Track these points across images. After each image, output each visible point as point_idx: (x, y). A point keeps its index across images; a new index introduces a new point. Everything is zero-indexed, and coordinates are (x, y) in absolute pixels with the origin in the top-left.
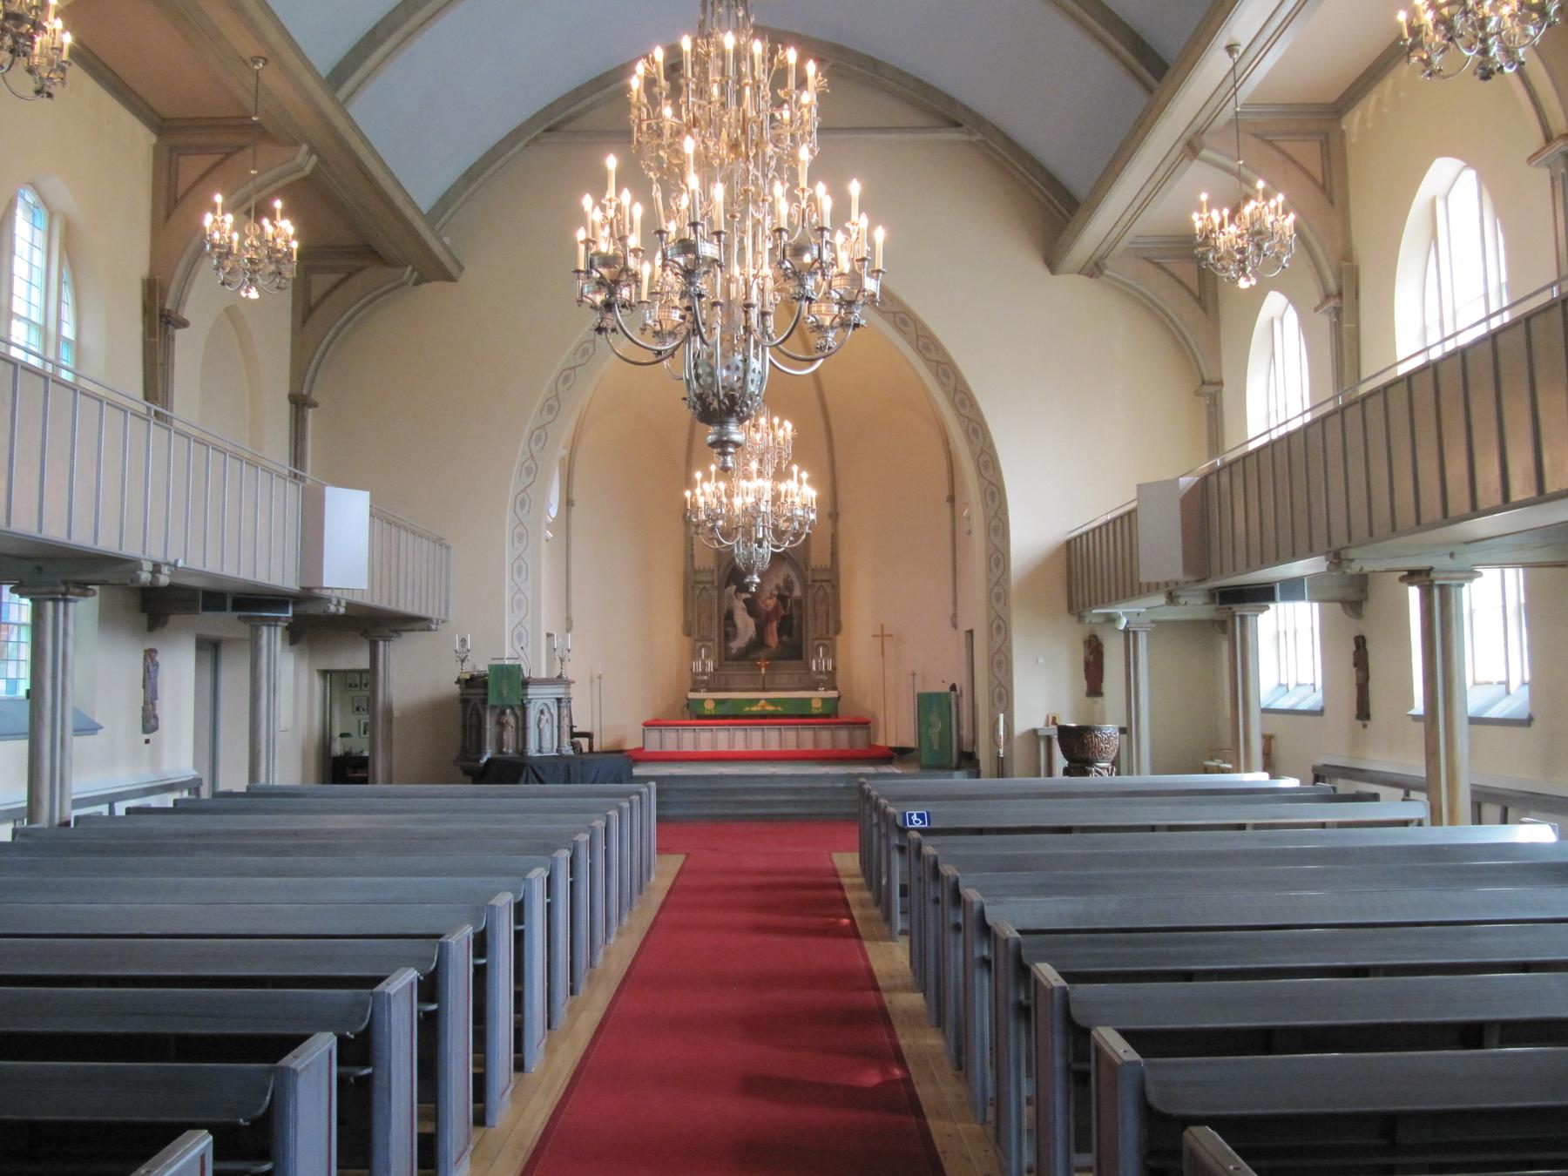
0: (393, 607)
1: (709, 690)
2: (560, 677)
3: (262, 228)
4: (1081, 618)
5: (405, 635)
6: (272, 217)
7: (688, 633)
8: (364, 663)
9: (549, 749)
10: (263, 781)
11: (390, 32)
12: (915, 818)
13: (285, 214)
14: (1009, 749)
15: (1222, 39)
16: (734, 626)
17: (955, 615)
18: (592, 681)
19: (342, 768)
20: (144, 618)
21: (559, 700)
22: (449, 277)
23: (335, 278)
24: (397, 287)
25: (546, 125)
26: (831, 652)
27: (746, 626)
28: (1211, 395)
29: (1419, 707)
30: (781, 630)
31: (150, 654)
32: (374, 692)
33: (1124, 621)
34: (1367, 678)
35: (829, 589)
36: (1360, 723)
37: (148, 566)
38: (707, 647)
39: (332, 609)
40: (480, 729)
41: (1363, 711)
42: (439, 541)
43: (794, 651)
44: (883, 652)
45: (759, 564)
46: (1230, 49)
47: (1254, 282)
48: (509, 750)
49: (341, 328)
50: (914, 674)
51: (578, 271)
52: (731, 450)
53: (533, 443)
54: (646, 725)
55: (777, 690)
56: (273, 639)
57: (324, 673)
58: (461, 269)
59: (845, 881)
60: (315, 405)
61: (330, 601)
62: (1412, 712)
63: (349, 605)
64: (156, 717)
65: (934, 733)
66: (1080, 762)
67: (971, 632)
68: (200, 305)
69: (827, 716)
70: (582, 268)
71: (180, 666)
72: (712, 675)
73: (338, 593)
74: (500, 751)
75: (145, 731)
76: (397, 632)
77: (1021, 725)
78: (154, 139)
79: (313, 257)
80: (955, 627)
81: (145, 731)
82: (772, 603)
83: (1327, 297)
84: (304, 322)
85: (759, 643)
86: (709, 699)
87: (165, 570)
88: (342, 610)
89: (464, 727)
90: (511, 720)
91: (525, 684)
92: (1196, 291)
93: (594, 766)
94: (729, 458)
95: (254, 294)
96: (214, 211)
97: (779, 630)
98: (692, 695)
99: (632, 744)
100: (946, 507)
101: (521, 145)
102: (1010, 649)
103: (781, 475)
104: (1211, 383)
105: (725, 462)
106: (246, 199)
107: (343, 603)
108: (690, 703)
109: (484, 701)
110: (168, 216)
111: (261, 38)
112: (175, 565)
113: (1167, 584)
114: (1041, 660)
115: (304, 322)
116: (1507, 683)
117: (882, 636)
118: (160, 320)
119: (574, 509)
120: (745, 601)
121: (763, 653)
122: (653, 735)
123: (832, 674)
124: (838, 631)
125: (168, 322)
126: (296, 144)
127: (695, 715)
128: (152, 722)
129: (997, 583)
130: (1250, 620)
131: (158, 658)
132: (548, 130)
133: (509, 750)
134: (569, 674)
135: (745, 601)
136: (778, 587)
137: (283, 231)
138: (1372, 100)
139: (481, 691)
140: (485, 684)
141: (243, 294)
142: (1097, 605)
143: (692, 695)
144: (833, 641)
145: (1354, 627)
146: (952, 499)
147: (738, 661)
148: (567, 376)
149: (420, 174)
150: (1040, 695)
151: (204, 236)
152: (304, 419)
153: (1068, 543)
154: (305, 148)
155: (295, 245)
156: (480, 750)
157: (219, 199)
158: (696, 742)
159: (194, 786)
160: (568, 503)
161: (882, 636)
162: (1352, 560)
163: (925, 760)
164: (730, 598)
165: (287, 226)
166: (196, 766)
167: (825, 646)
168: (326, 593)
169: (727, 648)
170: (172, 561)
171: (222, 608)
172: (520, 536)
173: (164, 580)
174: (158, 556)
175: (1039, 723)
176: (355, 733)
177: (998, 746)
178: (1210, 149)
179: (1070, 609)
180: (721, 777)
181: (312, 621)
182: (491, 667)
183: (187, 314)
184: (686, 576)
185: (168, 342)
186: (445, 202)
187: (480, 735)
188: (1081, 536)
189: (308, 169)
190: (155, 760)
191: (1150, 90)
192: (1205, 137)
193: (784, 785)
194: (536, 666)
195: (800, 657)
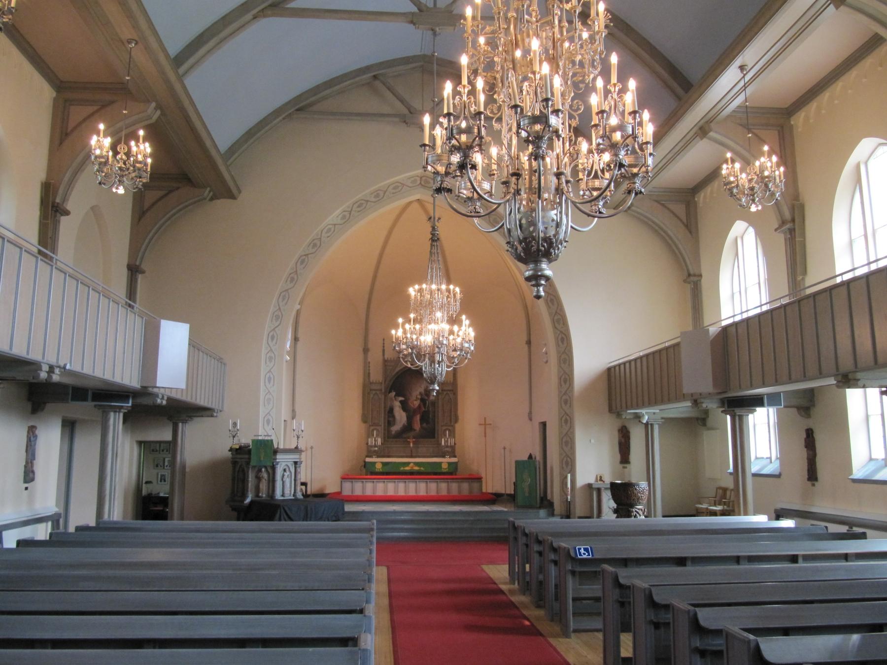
0: (193, 401)
1: (378, 457)
2: (297, 448)
3: (130, 148)
4: (619, 415)
5: (196, 419)
6: (137, 141)
7: (364, 420)
8: (167, 436)
9: (289, 495)
10: (106, 517)
11: (213, 36)
12: (582, 551)
13: (145, 139)
14: (573, 496)
15: (738, 62)
16: (394, 417)
17: (530, 413)
19: (150, 507)
20: (29, 406)
21: (296, 463)
22: (233, 197)
23: (161, 193)
24: (199, 201)
25: (297, 107)
26: (452, 434)
27: (401, 417)
28: (693, 284)
29: (731, 469)
30: (422, 420)
31: (32, 430)
32: (174, 457)
33: (646, 417)
34: (815, 455)
35: (451, 396)
36: (809, 483)
37: (45, 368)
38: (377, 430)
39: (159, 401)
40: (244, 481)
41: (812, 475)
42: (220, 360)
43: (430, 433)
44: (489, 437)
45: (439, 377)
46: (742, 68)
47: (760, 208)
48: (263, 495)
49: (163, 224)
50: (504, 448)
51: (425, 145)
52: (543, 282)
53: (281, 299)
55: (419, 457)
56: (116, 421)
57: (140, 443)
58: (240, 192)
59: (504, 587)
60: (143, 272)
61: (157, 396)
62: (851, 477)
63: (170, 399)
64: (33, 472)
65: (526, 485)
66: (624, 507)
67: (544, 425)
68: (78, 201)
69: (451, 474)
70: (427, 143)
71: (50, 438)
72: (379, 447)
73: (162, 391)
74: (257, 496)
75: (25, 481)
76: (191, 417)
77: (581, 481)
78: (54, 94)
79: (157, 175)
80: (531, 419)
81: (25, 481)
83: (783, 222)
84: (140, 219)
85: (408, 428)
86: (378, 462)
87: (57, 371)
88: (164, 402)
89: (233, 479)
90: (265, 475)
91: (275, 452)
92: (685, 221)
93: (317, 506)
94: (541, 289)
95: (121, 191)
96: (98, 135)
97: (421, 420)
98: (368, 460)
99: (331, 489)
100: (526, 347)
101: (281, 118)
102: (573, 433)
103: (454, 320)
104: (695, 275)
105: (538, 291)
106: (121, 130)
107: (165, 398)
108: (365, 464)
109: (248, 463)
110: (61, 143)
111: (136, 27)
112: (64, 368)
113: (692, 395)
114: (593, 441)
115: (140, 219)
116: (770, 458)
117: (485, 424)
118: (52, 209)
121: (412, 434)
122: (347, 485)
123: (453, 448)
124: (456, 421)
125: (56, 211)
126: (148, 101)
127: (368, 472)
128: (31, 475)
129: (565, 393)
130: (741, 417)
131: (37, 432)
132: (298, 110)
133: (263, 495)
134: (301, 446)
135: (401, 402)
136: (421, 394)
137: (142, 150)
138: (813, 106)
139: (247, 456)
140: (249, 452)
141: (114, 190)
142: (632, 408)
143: (368, 460)
144: (454, 427)
145: (805, 423)
146: (529, 342)
147: (396, 438)
148: (303, 260)
149: (222, 129)
150: (592, 462)
151: (90, 151)
152: (136, 282)
153: (609, 369)
154: (153, 105)
155: (149, 161)
156: (244, 496)
157: (102, 127)
158: (374, 489)
159: (55, 519)
160: (296, 339)
161: (485, 424)
162: (858, 380)
163: (520, 499)
164: (391, 399)
165: (147, 148)
166: (57, 505)
167: (449, 430)
168: (155, 390)
169: (389, 431)
170: (62, 364)
171: (85, 399)
172: (271, 358)
173: (56, 378)
174: (53, 360)
175: (591, 480)
176: (154, 481)
177: (567, 495)
178: (716, 132)
179: (610, 410)
180: (395, 512)
181: (148, 410)
182: (253, 441)
183: (69, 206)
185: (56, 224)
186: (233, 149)
187: (244, 488)
188: (619, 365)
189: (155, 117)
190: (31, 501)
191: (679, 98)
192: (712, 125)
193: (435, 518)
194: (280, 443)
195: (434, 437)
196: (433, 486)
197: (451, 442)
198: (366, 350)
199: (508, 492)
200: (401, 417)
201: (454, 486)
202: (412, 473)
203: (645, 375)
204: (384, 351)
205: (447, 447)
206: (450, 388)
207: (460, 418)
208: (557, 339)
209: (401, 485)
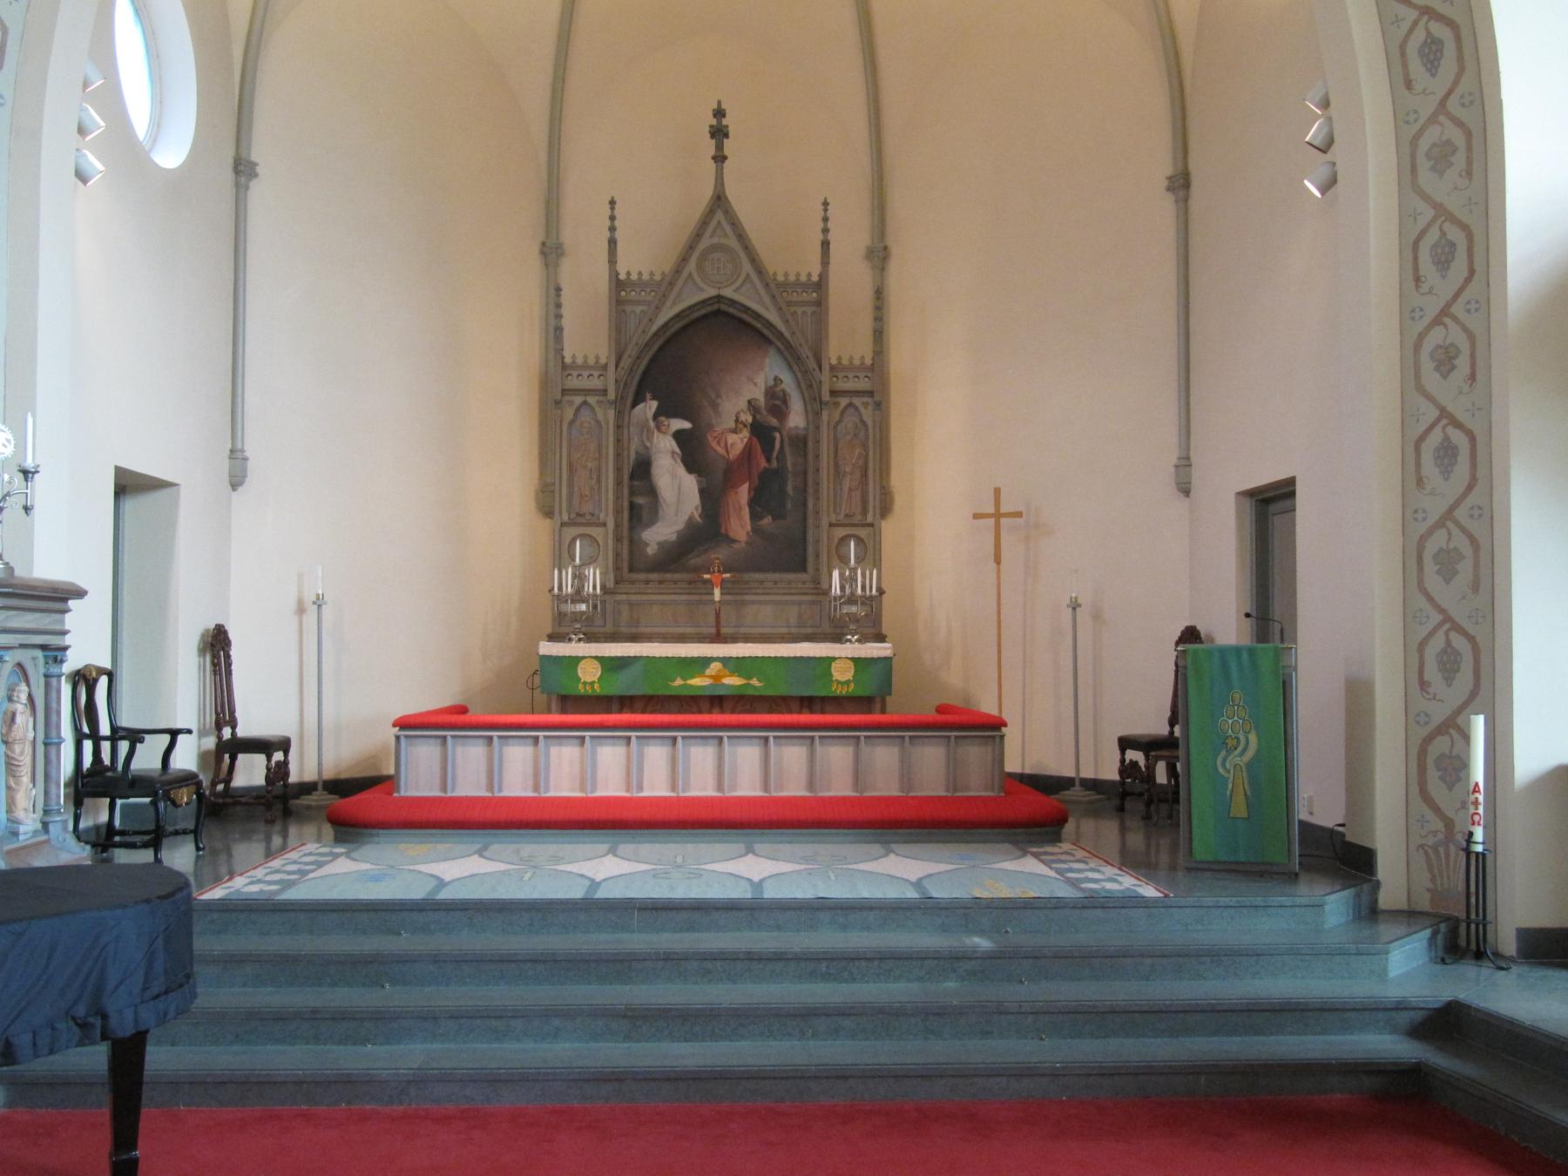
1: (590, 638)
7: (548, 512)
16: (652, 492)
17: (1184, 463)
18: (301, 610)
26: (871, 554)
27: (679, 492)
30: (758, 505)
43: (788, 553)
50: (1075, 606)
54: (404, 724)
67: (1270, 504)
82: (738, 442)
85: (705, 532)
98: (548, 648)
117: (998, 515)
119: (255, 186)
120: (679, 436)
121: (720, 554)
123: (873, 604)
124: (885, 509)
135: (679, 436)
146: (1181, 184)
147: (660, 571)
158: (538, 774)
163: (1205, 838)
164: (644, 427)
167: (859, 541)
169: (635, 545)
184: (545, 382)
196: (792, 757)
197: (867, 580)
198: (551, 252)
199: (1087, 773)
200: (679, 492)
201: (884, 757)
202: (717, 701)
203: (737, 766)
204: (612, 243)
205: (852, 600)
206: (863, 385)
207: (899, 501)
208: (1397, 56)
209: (656, 755)
